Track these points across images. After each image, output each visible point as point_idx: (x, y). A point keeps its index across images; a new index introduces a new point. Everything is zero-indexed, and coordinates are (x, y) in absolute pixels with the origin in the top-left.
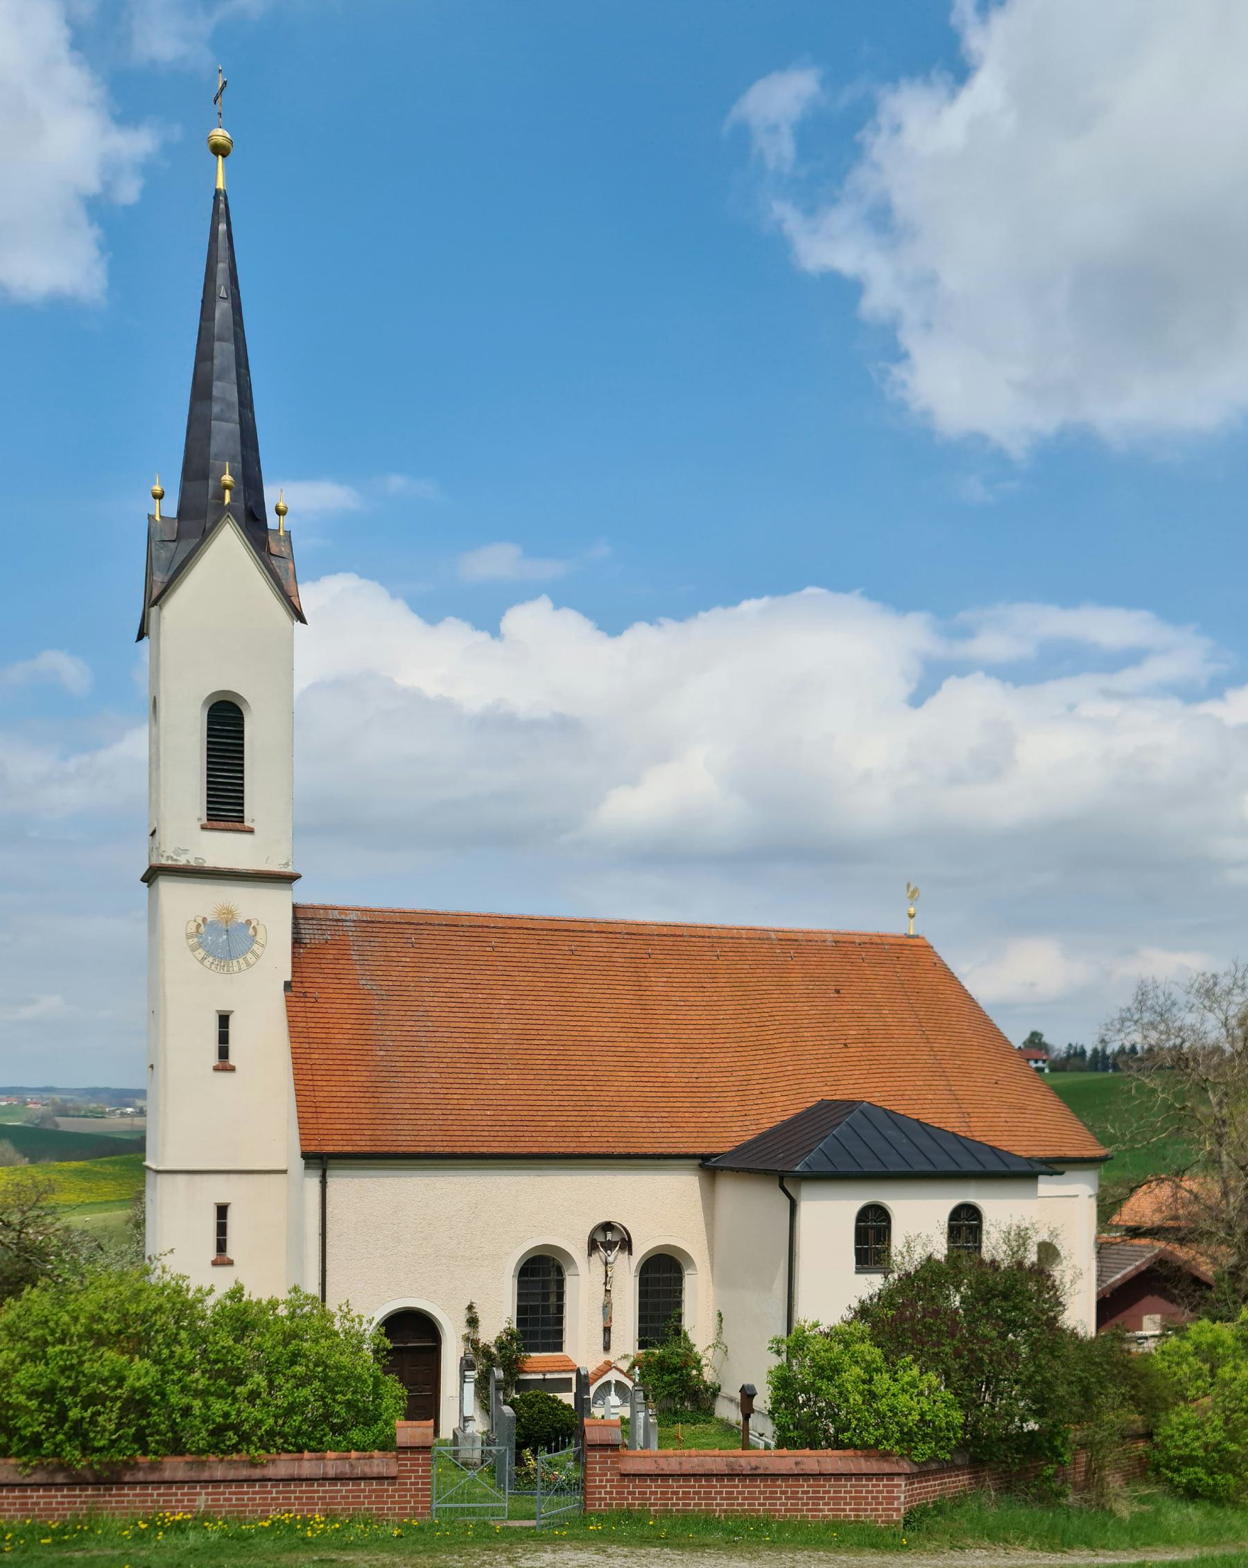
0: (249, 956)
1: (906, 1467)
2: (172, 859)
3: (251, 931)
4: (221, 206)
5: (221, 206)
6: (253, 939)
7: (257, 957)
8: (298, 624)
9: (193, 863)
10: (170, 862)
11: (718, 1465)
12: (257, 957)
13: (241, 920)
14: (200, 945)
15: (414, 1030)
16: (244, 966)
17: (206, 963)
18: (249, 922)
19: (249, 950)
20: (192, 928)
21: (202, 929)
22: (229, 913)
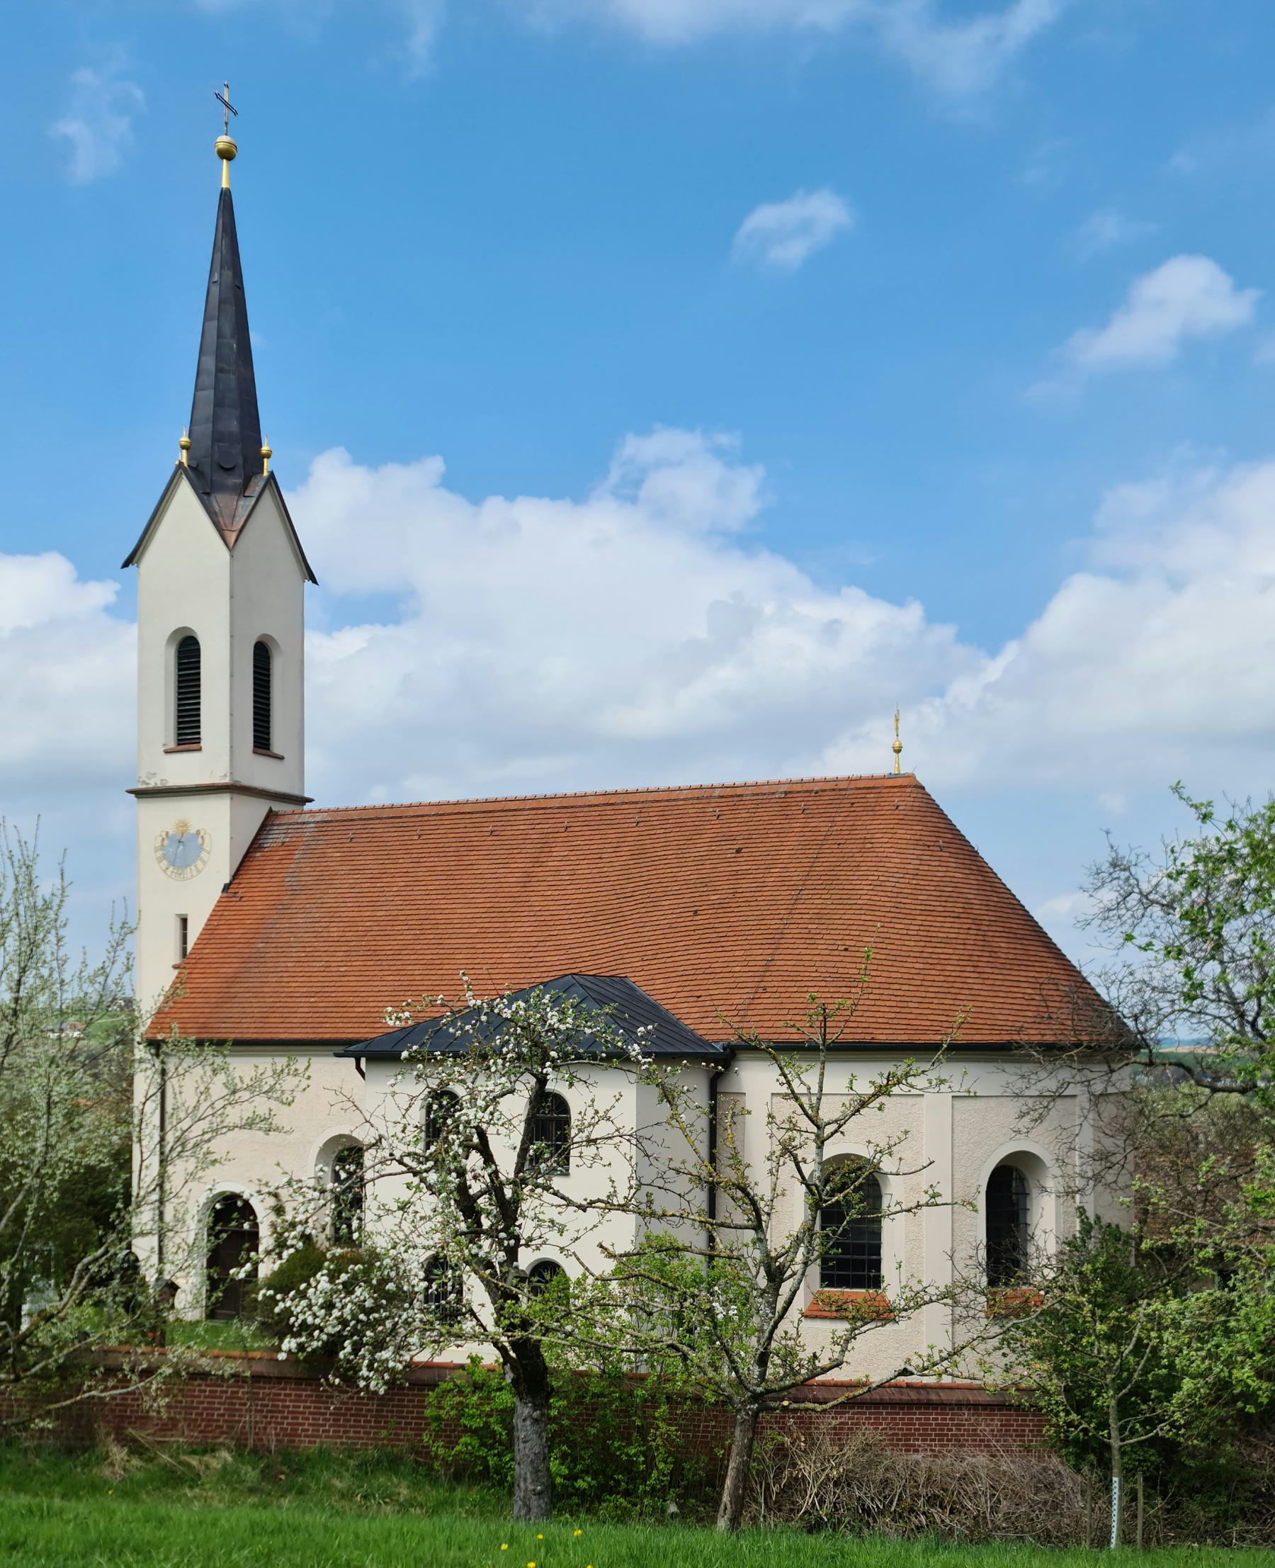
0: (199, 863)
1: (688, 1255)
2: (143, 782)
3: (200, 840)
4: (226, 199)
5: (226, 199)
6: (201, 848)
7: (205, 863)
8: (308, 583)
9: (159, 785)
10: (144, 786)
11: (152, 1107)
12: (205, 863)
13: (193, 831)
14: (164, 857)
15: (351, 919)
16: (195, 873)
17: (169, 872)
18: (198, 832)
19: (198, 857)
20: (159, 843)
21: (166, 843)
22: (184, 825)
